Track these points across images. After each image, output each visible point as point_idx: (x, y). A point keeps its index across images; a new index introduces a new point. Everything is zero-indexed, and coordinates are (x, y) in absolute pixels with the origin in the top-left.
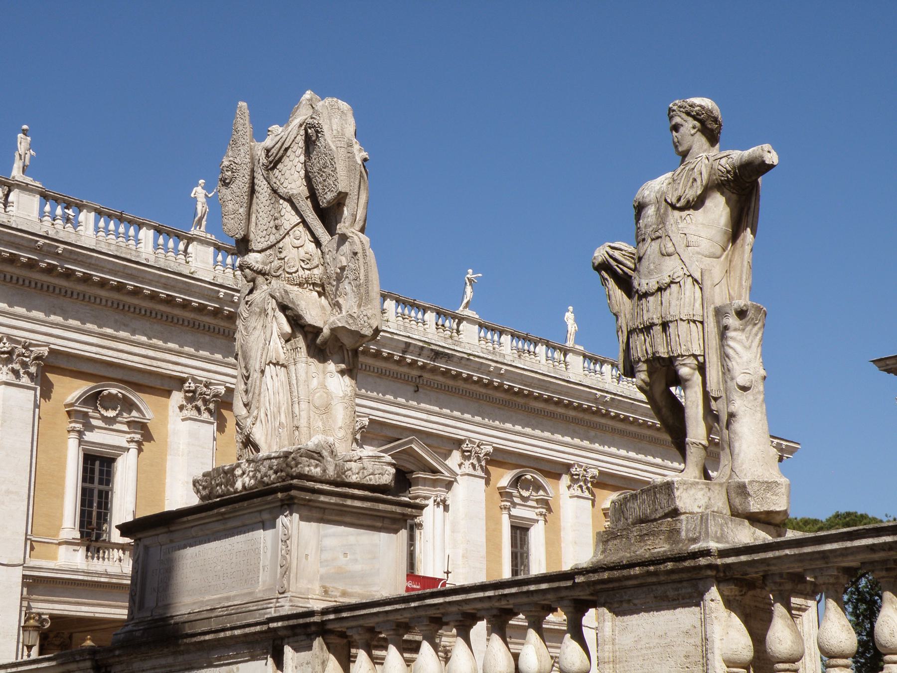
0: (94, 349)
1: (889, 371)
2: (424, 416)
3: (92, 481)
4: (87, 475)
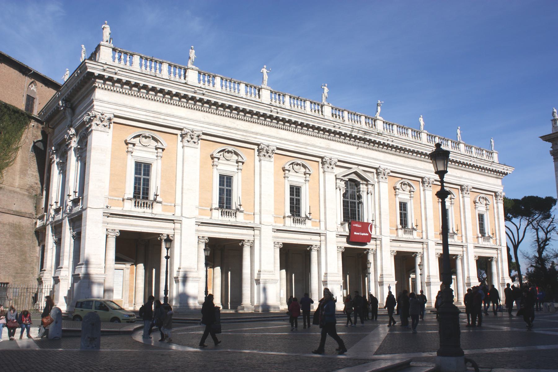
0: (230, 134)
1: (546, 141)
2: (361, 159)
3: (293, 195)
4: (221, 183)
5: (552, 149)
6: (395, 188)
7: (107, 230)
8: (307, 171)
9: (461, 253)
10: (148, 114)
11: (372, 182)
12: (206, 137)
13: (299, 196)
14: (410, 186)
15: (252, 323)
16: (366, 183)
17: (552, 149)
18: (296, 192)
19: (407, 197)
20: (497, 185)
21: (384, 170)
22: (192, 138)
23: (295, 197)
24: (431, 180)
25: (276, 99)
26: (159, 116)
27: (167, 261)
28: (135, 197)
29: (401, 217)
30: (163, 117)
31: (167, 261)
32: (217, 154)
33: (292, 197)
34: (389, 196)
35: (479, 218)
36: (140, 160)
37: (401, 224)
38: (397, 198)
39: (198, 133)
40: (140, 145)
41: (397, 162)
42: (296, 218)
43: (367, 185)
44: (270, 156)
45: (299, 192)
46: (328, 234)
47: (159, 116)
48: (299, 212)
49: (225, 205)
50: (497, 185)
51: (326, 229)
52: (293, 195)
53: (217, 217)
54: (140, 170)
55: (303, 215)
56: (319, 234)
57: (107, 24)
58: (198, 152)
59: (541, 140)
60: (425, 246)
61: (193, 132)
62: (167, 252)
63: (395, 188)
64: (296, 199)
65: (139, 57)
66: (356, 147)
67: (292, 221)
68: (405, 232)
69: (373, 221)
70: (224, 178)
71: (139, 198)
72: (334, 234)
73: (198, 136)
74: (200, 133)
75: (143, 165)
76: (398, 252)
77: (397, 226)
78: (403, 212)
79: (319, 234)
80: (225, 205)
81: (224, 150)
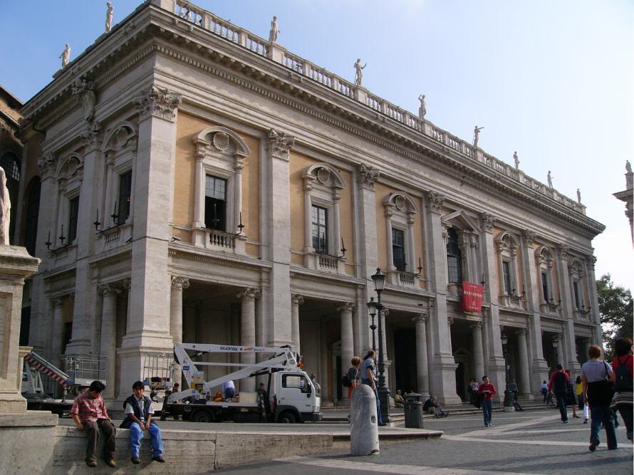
1: (620, 199)
5: (626, 210)
7: (172, 277)
10: (226, 102)
11: (476, 232)
12: (193, 111)
14: (333, 177)
15: (339, 428)
16: (468, 232)
17: (626, 210)
19: (404, 222)
20: (158, 80)
26: (240, 107)
27: (373, 332)
30: (245, 110)
31: (373, 332)
43: (470, 235)
47: (240, 107)
50: (158, 80)
59: (614, 197)
62: (373, 320)
66: (459, 183)
68: (403, 278)
69: (420, 268)
73: (175, 103)
76: (193, 282)
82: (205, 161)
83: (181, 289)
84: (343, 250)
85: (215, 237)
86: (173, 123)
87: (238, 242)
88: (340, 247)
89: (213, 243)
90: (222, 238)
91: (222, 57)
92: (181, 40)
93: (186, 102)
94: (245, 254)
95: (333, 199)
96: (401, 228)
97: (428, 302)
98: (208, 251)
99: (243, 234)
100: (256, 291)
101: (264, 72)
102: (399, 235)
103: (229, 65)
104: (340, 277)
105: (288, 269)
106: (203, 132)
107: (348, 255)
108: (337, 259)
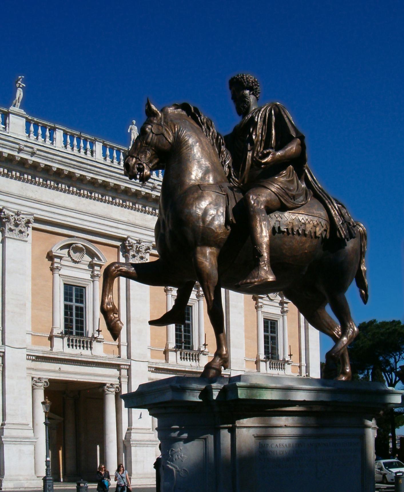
4: (68, 296)
6: (50, 257)
7: (33, 378)
8: (96, 261)
9: (116, 381)
12: (44, 225)
13: (82, 302)
14: (92, 254)
18: (271, 327)
21: (18, 214)
22: (17, 225)
23: (74, 304)
24: (144, 245)
25: (112, 157)
28: (66, 333)
29: (266, 342)
32: (59, 251)
33: (266, 334)
34: (35, 269)
35: (66, 293)
36: (71, 282)
37: (266, 352)
38: (260, 312)
39: (27, 218)
40: (268, 299)
41: (57, 202)
42: (273, 361)
44: (21, 232)
45: (274, 328)
46: (134, 366)
48: (189, 343)
49: (74, 330)
51: (129, 357)
52: (71, 300)
53: (60, 347)
54: (71, 295)
55: (196, 348)
56: (118, 367)
57: (135, 125)
58: (27, 247)
60: (124, 372)
61: (140, 243)
63: (50, 257)
64: (77, 308)
65: (101, 144)
67: (179, 356)
70: (71, 290)
71: (71, 333)
72: (144, 367)
73: (28, 222)
74: (31, 218)
75: (74, 288)
77: (258, 356)
78: (269, 334)
79: (118, 367)
80: (74, 330)
81: (71, 244)
82: (63, 272)
83: (43, 388)
84: (290, 355)
85: (83, 343)
86: (26, 241)
87: (95, 344)
88: (287, 353)
89: (183, 360)
90: (80, 341)
91: (55, 169)
92: (82, 177)
93: (37, 220)
94: (104, 355)
95: (282, 313)
96: (274, 318)
97: (119, 370)
98: (66, 354)
99: (101, 336)
100: (115, 386)
101: (89, 176)
102: (271, 326)
103: (63, 176)
104: (97, 357)
105: (25, 352)
106: (56, 245)
107: (296, 356)
108: (285, 362)
